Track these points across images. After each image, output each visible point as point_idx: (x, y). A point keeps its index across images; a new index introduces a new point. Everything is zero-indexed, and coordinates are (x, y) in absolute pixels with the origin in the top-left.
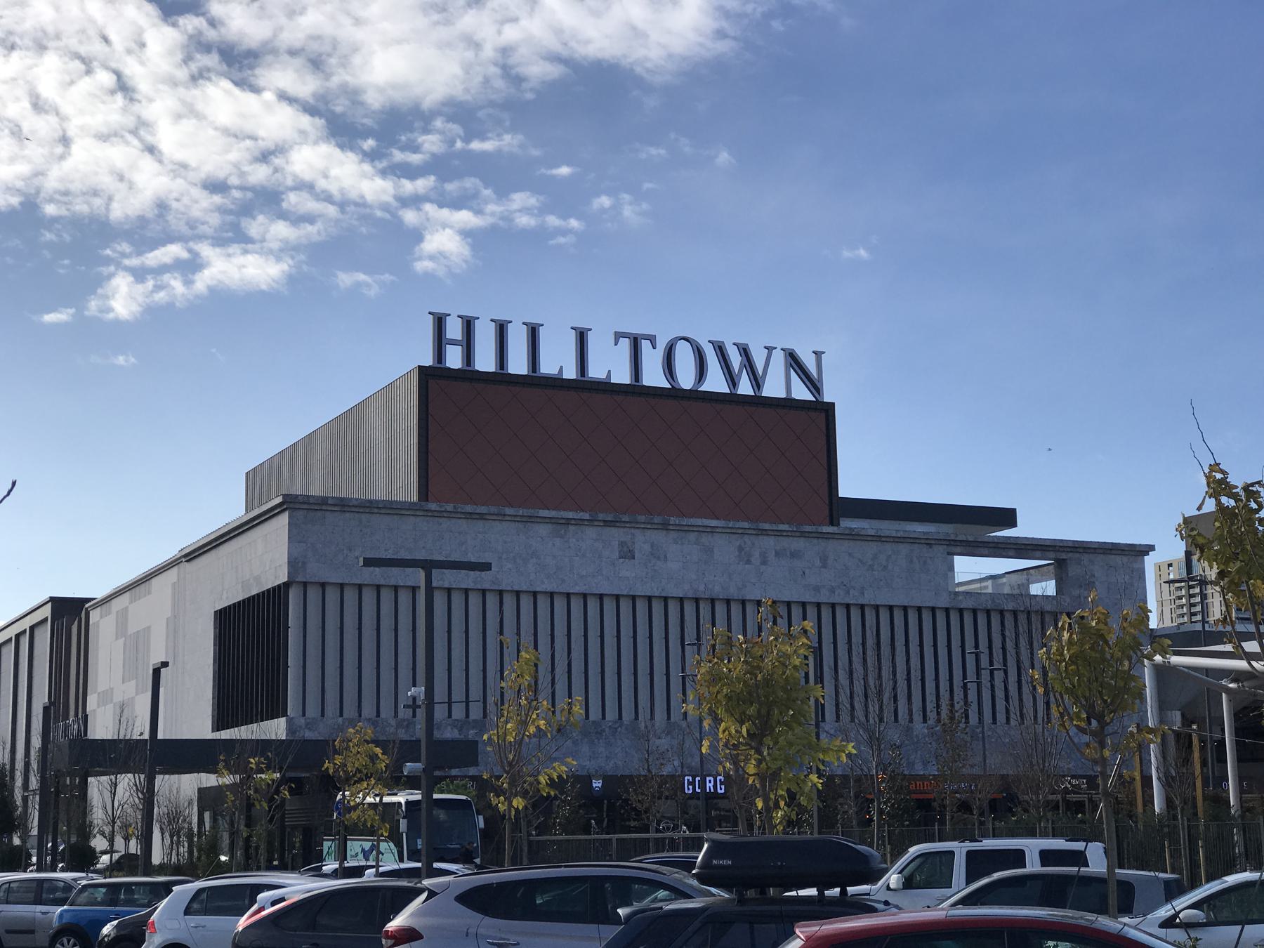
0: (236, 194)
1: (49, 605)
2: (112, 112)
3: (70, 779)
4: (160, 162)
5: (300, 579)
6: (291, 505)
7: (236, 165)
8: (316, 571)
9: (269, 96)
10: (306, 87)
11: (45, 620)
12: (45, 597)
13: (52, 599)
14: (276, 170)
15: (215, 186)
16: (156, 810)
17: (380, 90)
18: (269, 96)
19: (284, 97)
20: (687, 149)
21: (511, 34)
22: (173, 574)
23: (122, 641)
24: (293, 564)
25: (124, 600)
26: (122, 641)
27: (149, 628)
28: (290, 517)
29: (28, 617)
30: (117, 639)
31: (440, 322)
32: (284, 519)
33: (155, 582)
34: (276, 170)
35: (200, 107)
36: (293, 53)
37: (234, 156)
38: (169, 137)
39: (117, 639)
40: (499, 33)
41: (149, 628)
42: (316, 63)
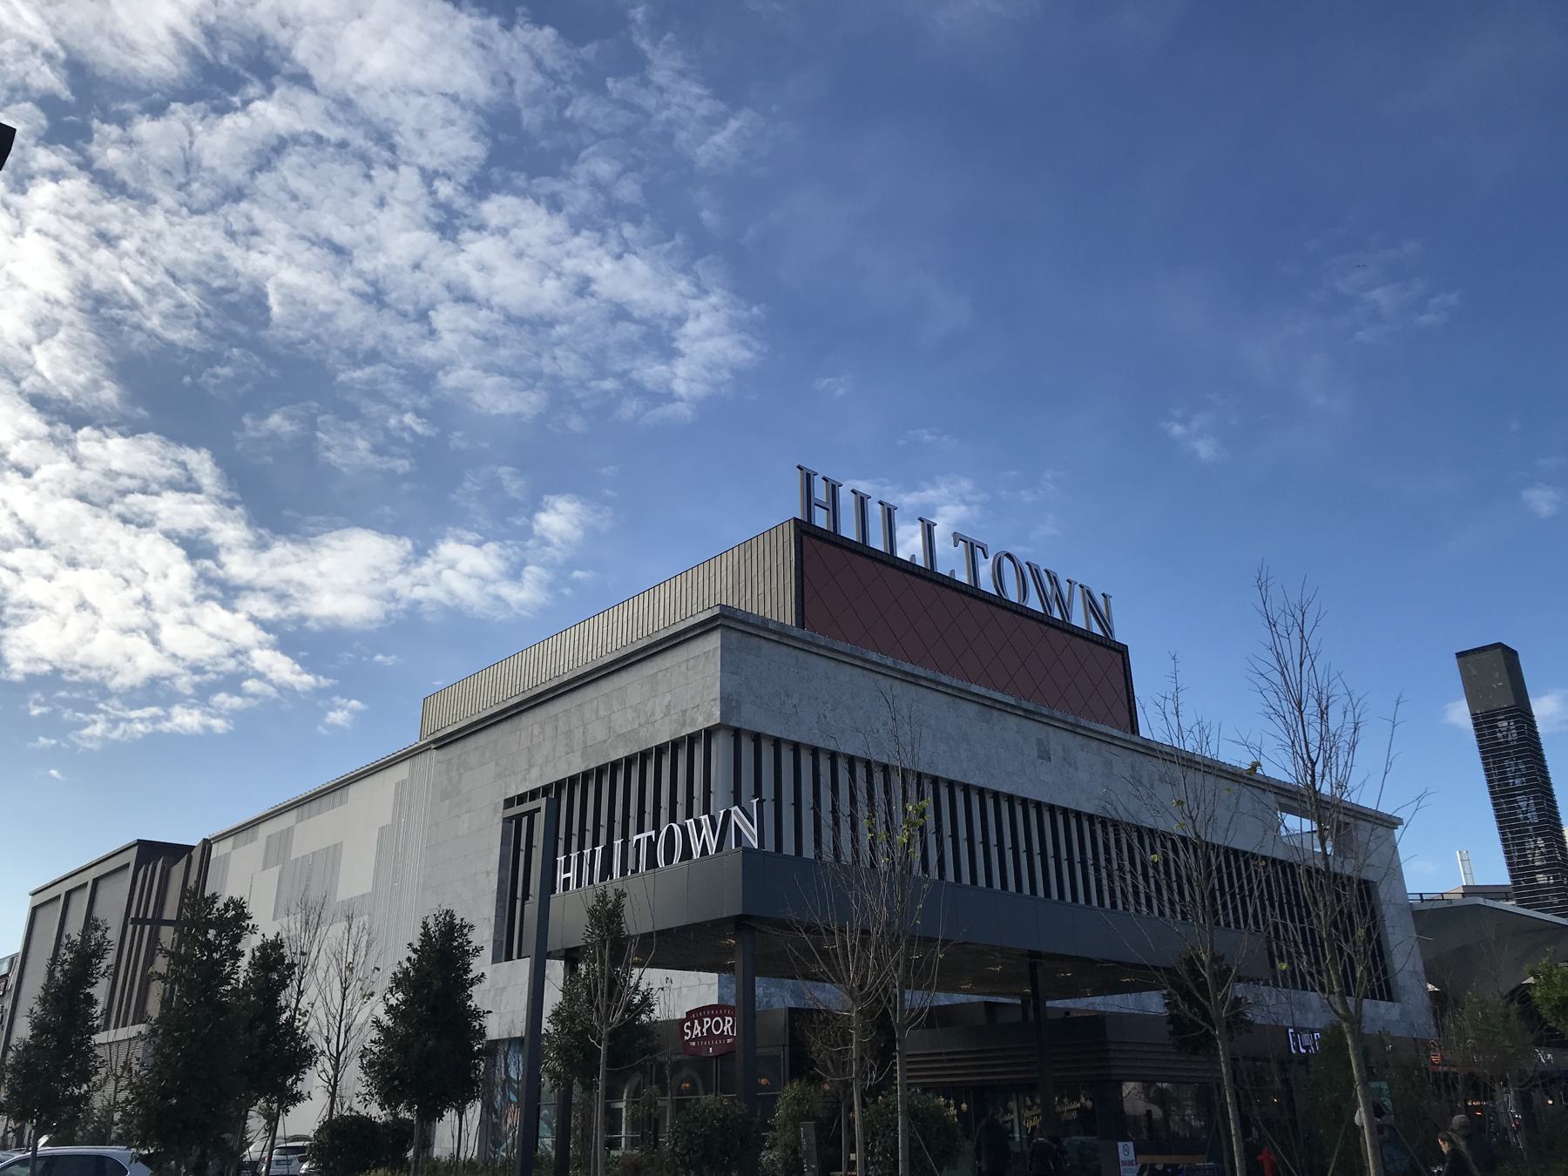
0: (212, 676)
1: (135, 850)
2: (136, 617)
3: (1018, 1005)
4: (160, 651)
5: (734, 723)
6: (726, 622)
7: (213, 657)
8: (753, 719)
9: (241, 616)
10: (270, 611)
11: (127, 865)
12: (132, 839)
13: (140, 842)
14: (241, 663)
15: (196, 669)
16: (573, 1121)
17: (319, 620)
18: (241, 616)
19: (254, 619)
20: (927, 437)
21: (419, 593)
22: (402, 771)
23: (275, 870)
24: (728, 701)
25: (289, 819)
26: (275, 870)
27: (337, 847)
28: (722, 637)
29: (93, 868)
30: (265, 868)
31: (808, 478)
32: (714, 641)
33: (354, 790)
34: (241, 663)
35: (196, 620)
36: (264, 590)
37: (212, 651)
38: (171, 635)
39: (265, 868)
40: (411, 591)
41: (337, 847)
42: (281, 597)
